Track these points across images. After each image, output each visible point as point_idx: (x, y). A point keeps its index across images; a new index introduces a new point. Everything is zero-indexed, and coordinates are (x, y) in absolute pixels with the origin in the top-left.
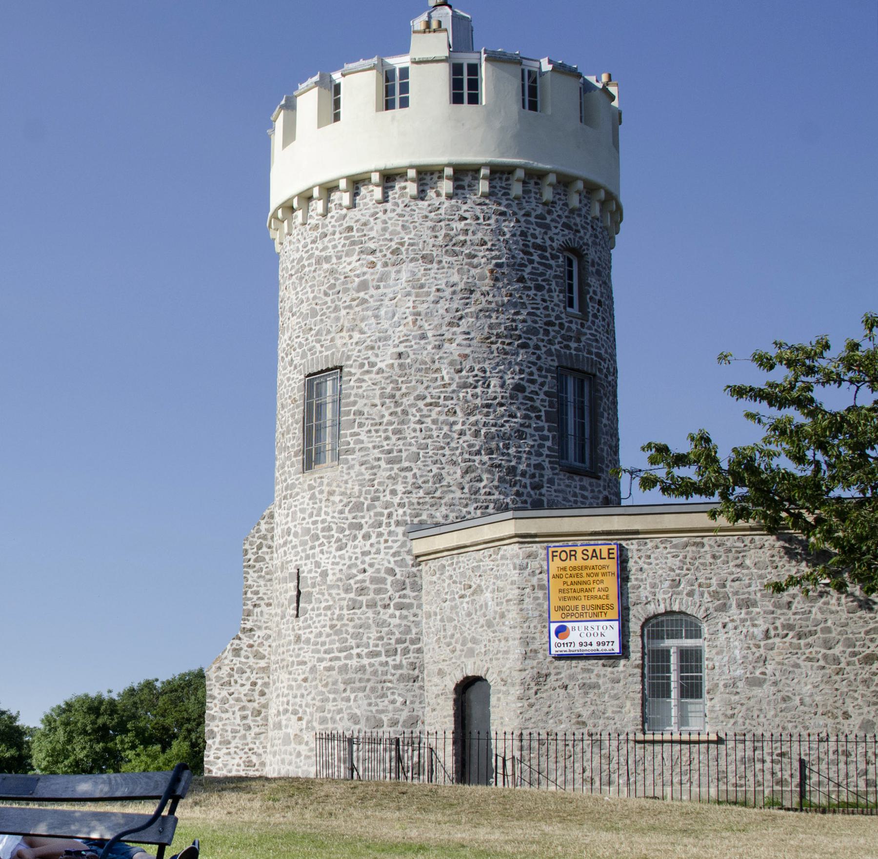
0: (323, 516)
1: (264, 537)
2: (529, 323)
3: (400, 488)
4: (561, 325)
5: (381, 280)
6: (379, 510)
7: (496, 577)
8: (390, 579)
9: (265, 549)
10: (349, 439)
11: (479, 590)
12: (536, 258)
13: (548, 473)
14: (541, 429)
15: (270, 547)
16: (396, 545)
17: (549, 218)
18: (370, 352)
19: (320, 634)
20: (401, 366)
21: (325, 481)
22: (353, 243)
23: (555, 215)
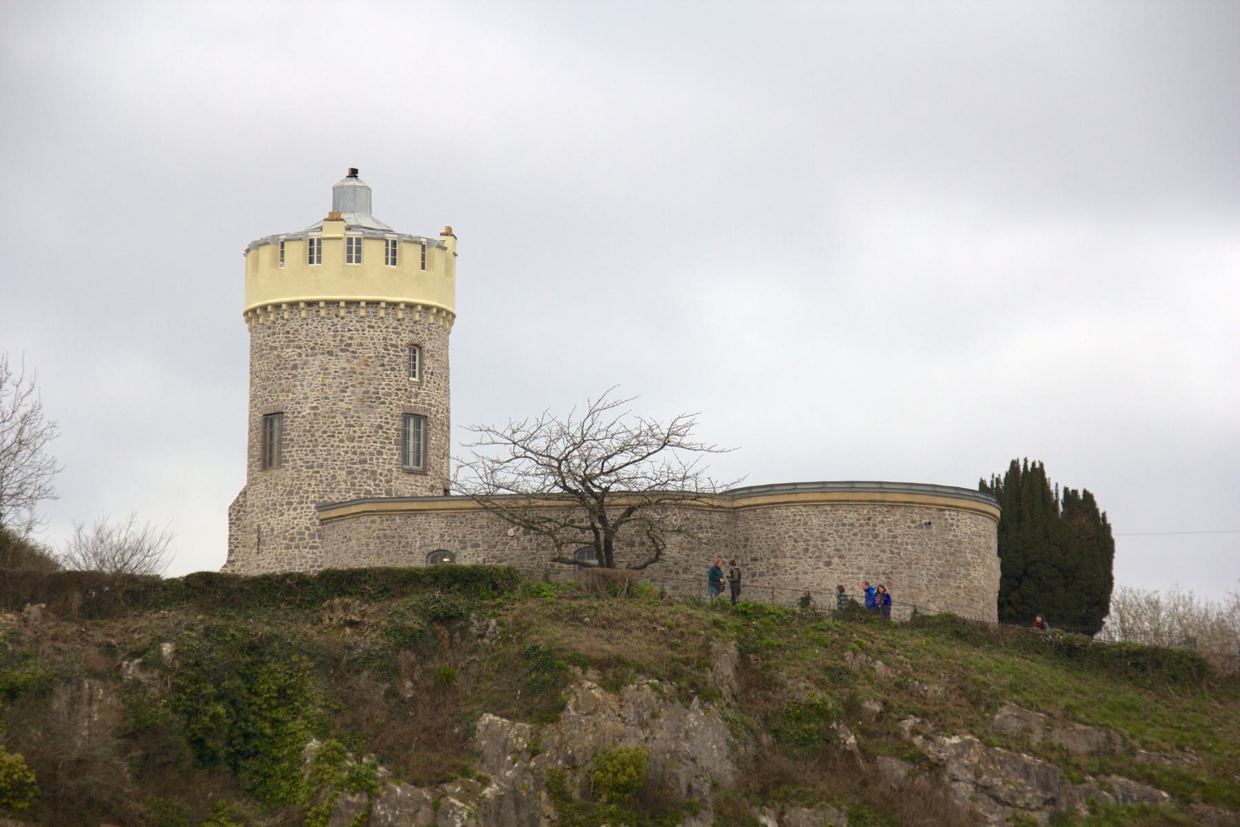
0: (272, 497)
1: (241, 506)
2: (386, 390)
3: (313, 482)
4: (406, 390)
5: (304, 364)
6: (301, 494)
7: (358, 533)
8: (307, 532)
9: (241, 513)
10: (286, 454)
11: (350, 539)
12: (391, 352)
13: (395, 474)
14: (392, 449)
15: (245, 512)
16: (310, 514)
17: (400, 328)
18: (298, 406)
19: (270, 563)
20: (315, 414)
21: (273, 477)
22: (290, 341)
23: (404, 327)
